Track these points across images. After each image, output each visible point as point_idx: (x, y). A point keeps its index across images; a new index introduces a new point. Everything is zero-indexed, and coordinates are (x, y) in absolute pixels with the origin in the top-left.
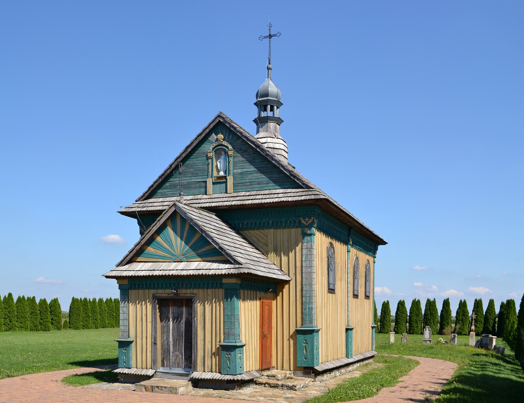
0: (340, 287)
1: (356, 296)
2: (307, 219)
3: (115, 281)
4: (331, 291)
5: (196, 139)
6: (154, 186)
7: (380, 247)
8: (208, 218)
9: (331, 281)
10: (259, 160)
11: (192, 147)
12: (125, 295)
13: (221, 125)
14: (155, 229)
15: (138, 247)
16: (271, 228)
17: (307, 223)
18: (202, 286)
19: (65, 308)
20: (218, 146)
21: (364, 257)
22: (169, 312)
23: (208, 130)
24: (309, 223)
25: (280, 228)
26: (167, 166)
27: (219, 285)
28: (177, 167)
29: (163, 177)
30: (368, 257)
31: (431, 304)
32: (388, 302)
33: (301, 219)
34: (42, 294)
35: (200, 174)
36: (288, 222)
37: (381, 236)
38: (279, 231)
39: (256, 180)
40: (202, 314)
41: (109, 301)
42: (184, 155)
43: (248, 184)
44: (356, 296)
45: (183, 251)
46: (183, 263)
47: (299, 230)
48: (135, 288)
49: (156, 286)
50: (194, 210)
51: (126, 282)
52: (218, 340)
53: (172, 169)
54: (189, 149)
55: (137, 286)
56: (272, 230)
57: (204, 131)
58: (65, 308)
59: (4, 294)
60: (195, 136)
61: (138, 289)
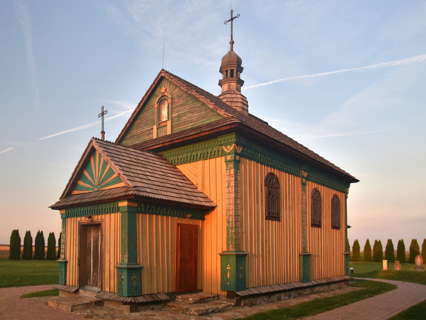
2: (229, 147)
3: (58, 212)
5: (146, 95)
7: (352, 185)
10: (191, 102)
11: (136, 113)
16: (200, 160)
17: (228, 150)
20: (162, 97)
23: (154, 86)
29: (125, 131)
33: (224, 147)
35: (150, 123)
37: (352, 174)
38: (207, 162)
39: (189, 120)
42: (138, 110)
45: (100, 179)
47: (223, 158)
48: (69, 218)
52: (116, 263)
54: (142, 105)
56: (200, 162)
59: (6, 240)
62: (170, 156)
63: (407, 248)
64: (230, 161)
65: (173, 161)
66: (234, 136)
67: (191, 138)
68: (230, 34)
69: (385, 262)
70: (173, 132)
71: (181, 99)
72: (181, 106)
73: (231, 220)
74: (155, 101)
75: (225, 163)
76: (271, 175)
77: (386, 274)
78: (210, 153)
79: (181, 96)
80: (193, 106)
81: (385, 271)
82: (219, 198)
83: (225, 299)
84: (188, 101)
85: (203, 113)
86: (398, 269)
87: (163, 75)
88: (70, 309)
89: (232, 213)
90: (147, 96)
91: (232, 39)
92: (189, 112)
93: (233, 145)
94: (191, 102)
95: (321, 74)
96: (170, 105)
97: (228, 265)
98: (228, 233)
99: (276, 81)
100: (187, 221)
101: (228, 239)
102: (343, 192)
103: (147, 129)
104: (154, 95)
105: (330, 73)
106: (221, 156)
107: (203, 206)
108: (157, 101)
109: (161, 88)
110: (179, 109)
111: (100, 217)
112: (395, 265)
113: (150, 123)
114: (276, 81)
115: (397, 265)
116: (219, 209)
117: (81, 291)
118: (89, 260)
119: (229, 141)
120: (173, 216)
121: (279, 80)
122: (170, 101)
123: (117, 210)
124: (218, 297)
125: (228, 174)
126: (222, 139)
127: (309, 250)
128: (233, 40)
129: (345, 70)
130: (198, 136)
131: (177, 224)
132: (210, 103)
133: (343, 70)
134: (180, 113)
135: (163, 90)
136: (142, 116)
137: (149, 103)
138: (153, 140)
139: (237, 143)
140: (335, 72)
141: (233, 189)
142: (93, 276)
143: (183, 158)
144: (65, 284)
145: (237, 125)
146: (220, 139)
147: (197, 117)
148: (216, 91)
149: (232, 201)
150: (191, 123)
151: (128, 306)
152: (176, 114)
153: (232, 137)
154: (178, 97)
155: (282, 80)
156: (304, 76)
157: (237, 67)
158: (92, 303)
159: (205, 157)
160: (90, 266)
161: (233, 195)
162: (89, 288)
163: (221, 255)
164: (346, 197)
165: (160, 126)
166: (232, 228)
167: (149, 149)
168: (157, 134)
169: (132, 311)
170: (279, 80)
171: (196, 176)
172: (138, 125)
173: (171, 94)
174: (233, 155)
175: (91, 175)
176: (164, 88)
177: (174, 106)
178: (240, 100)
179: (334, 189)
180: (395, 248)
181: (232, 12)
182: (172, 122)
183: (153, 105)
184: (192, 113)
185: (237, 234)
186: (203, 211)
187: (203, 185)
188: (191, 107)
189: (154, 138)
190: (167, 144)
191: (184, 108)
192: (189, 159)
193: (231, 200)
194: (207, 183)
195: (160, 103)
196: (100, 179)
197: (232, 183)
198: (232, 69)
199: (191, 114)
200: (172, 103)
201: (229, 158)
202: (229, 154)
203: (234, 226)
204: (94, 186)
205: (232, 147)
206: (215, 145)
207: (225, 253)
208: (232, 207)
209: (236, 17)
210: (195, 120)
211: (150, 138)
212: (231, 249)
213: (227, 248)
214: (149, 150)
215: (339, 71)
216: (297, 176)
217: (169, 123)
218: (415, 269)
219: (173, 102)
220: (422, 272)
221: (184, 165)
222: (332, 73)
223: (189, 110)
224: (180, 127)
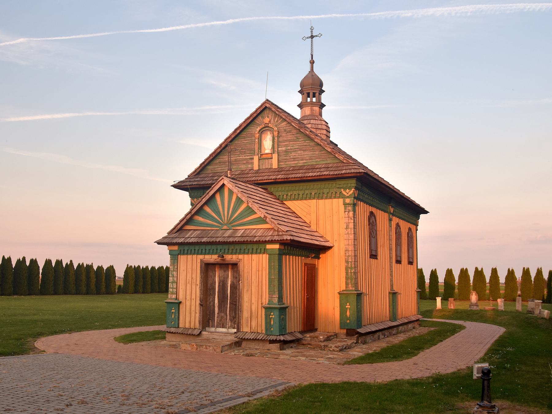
0: (383, 252)
1: (399, 262)
2: (348, 191)
3: (166, 247)
4: (374, 256)
5: (244, 122)
6: (206, 163)
7: (422, 216)
8: (254, 191)
9: (373, 248)
10: (302, 139)
12: (174, 260)
13: (267, 108)
14: (204, 200)
15: (188, 217)
16: (314, 198)
18: (246, 251)
19: (120, 273)
20: (264, 127)
21: (405, 226)
22: (215, 276)
25: (322, 198)
26: (217, 145)
27: (263, 251)
28: (226, 146)
30: (409, 225)
31: (479, 273)
32: (435, 269)
33: (342, 190)
34: (98, 260)
35: (248, 152)
36: (330, 193)
37: (422, 205)
41: (161, 268)
42: (233, 136)
44: (399, 262)
45: (231, 217)
46: (239, 235)
47: (341, 200)
48: (184, 254)
49: (204, 251)
50: (241, 183)
51: (176, 248)
54: (238, 131)
55: (186, 252)
56: (314, 201)
58: (120, 273)
61: (187, 254)
62: (277, 191)
63: (441, 279)
64: (348, 204)
69: (439, 300)
72: (290, 141)
73: (350, 260)
76: (372, 213)
77: (442, 313)
78: (326, 193)
80: (305, 144)
81: (439, 310)
82: (336, 237)
83: (345, 337)
85: (317, 153)
86: (452, 307)
87: (268, 105)
88: (219, 350)
89: (351, 253)
91: (312, 58)
93: (353, 189)
94: (302, 139)
95: (304, 17)
96: (276, 138)
97: (348, 304)
98: (347, 273)
99: (237, 20)
100: (309, 261)
101: (347, 278)
102: (414, 224)
105: (317, 17)
106: (339, 198)
107: (324, 246)
109: (263, 118)
111: (234, 257)
112: (449, 302)
113: (248, 152)
114: (237, 20)
115: (451, 303)
116: (335, 249)
117: (204, 333)
118: (211, 300)
119: (349, 185)
120: (302, 256)
121: (241, 19)
122: (276, 134)
123: (265, 251)
124: (336, 335)
125: (347, 216)
127: (396, 289)
129: (338, 15)
131: (305, 264)
132: (327, 145)
133: (334, 15)
134: (289, 148)
135: (267, 120)
136: (237, 142)
139: (356, 188)
140: (323, 16)
141: (352, 230)
142: (218, 317)
144: (178, 327)
145: (362, 174)
148: (297, 113)
149: (351, 242)
150: (302, 160)
151: (278, 345)
152: (284, 149)
153: (353, 182)
154: (285, 131)
155: (247, 19)
156: (279, 17)
158: (232, 343)
159: (320, 197)
160: (214, 306)
161: (352, 237)
162: (213, 329)
163: (339, 293)
164: (417, 230)
166: (351, 268)
167: (256, 182)
168: (259, 166)
169: (281, 349)
170: (241, 19)
171: (310, 214)
173: (276, 126)
174: (353, 198)
176: (268, 119)
177: (281, 139)
178: (324, 127)
179: (408, 222)
180: (427, 280)
181: (312, 29)
183: (252, 134)
184: (304, 151)
185: (353, 275)
186: (319, 250)
187: (317, 224)
188: (302, 144)
192: (301, 196)
193: (350, 241)
194: (321, 222)
196: (231, 217)
197: (351, 226)
198: (312, 88)
199: (302, 152)
201: (348, 201)
202: (348, 197)
203: (353, 266)
204: (221, 224)
205: (352, 192)
207: (345, 292)
208: (351, 248)
210: (307, 158)
212: (351, 288)
213: (346, 287)
215: (329, 16)
216: (385, 211)
217: (275, 156)
218: (470, 307)
220: (477, 310)
221: (294, 202)
222: (320, 17)
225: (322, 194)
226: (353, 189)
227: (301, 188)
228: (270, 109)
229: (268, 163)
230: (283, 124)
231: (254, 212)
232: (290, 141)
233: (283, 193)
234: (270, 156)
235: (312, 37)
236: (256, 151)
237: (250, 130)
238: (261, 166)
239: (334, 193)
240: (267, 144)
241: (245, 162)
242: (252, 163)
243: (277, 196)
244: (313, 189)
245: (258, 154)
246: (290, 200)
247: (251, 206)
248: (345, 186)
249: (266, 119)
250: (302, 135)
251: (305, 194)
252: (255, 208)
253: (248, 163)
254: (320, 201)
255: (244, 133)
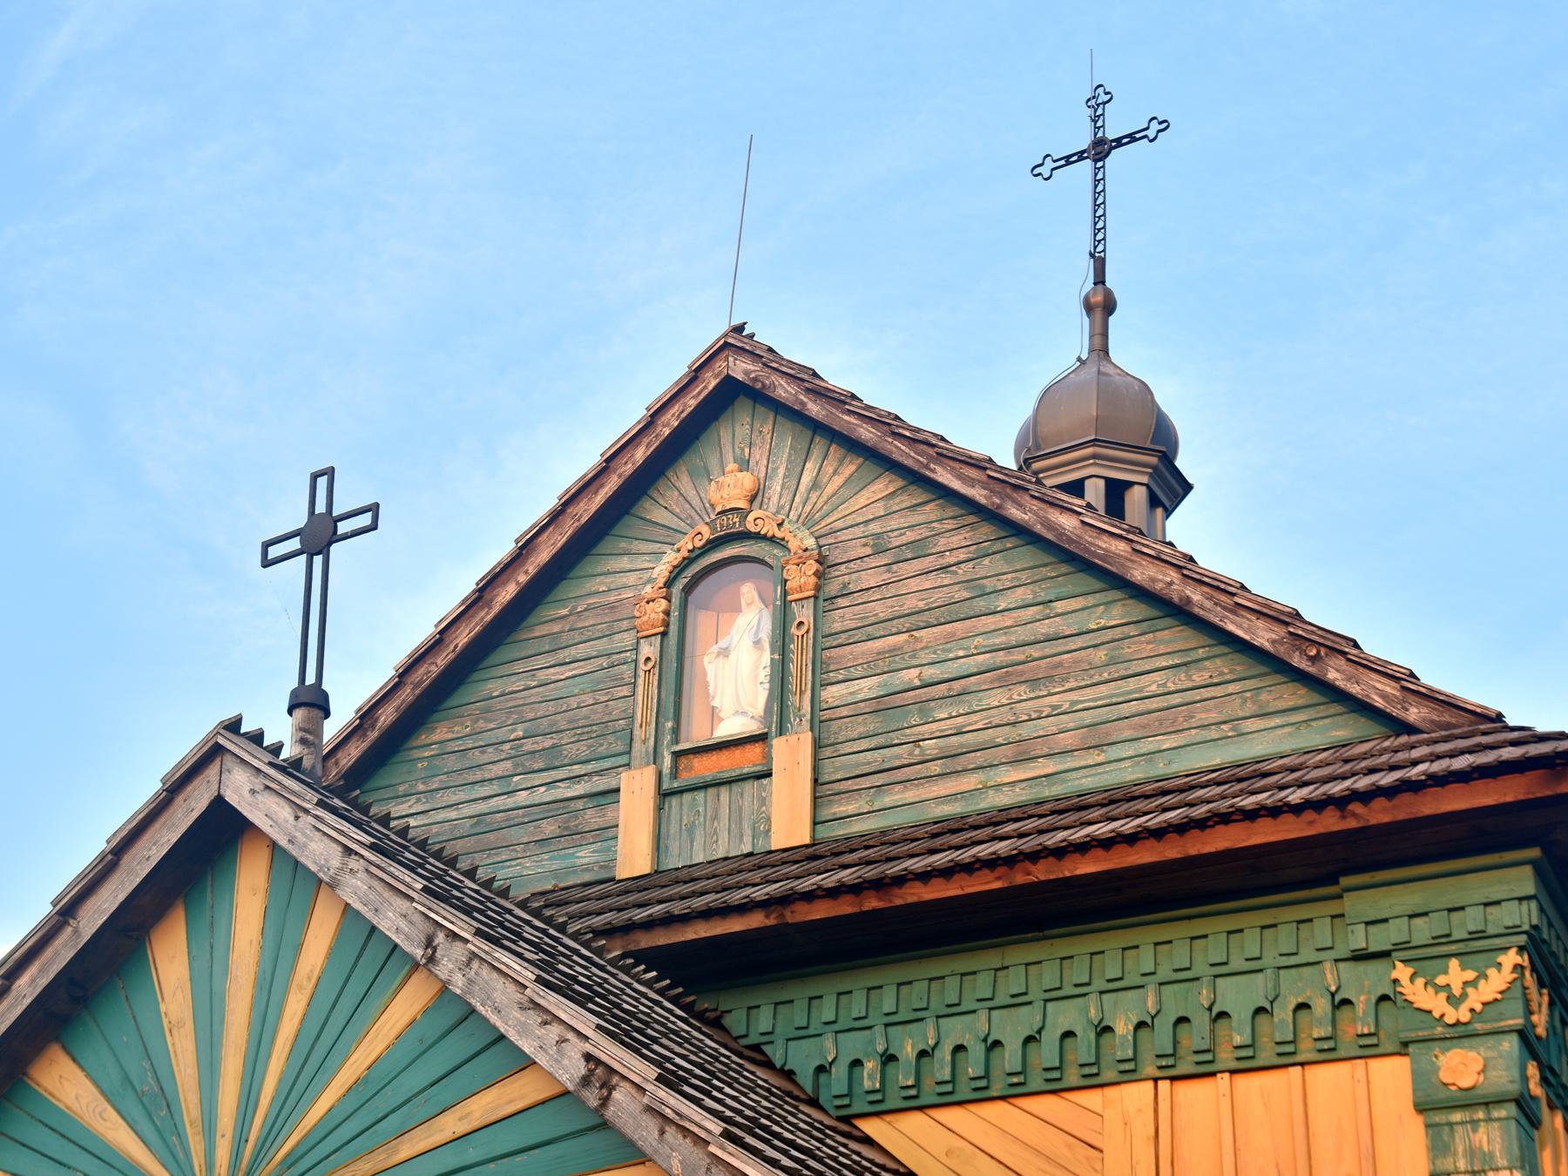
5: (555, 516)
11: (442, 660)
16: (1129, 1073)
17: (1454, 1001)
23: (640, 454)
24: (1475, 1000)
33: (1402, 972)
40: (961, 746)
42: (463, 637)
43: (935, 768)
53: (373, 735)
54: (507, 593)
56: (1137, 1095)
57: (401, 676)
60: (551, 502)
64: (1474, 1101)
65: (840, 1072)
66: (1523, 881)
67: (1086, 866)
68: (1087, 246)
70: (825, 832)
71: (917, 565)
72: (917, 620)
74: (637, 573)
75: (1415, 1126)
79: (918, 549)
80: (1044, 628)
84: (989, 584)
87: (740, 368)
90: (568, 528)
91: (1100, 279)
92: (1004, 675)
93: (1511, 958)
96: (804, 613)
103: (543, 795)
104: (628, 525)
106: (1369, 1049)
108: (662, 570)
110: (894, 651)
113: (582, 750)
122: (802, 577)
126: (1388, 906)
128: (1110, 282)
130: (1171, 850)
135: (730, 487)
136: (495, 687)
137: (566, 590)
138: (607, 887)
143: (945, 1053)
146: (1360, 904)
147: (1088, 718)
152: (867, 687)
153: (1506, 893)
154: (879, 551)
157: (1156, 473)
165: (686, 778)
172: (452, 762)
173: (808, 522)
175: (152, 1105)
176: (747, 480)
177: (839, 620)
181: (1098, 103)
182: (818, 745)
184: (1033, 682)
189: (623, 872)
190: (820, 911)
191: (951, 639)
192: (1010, 1057)
195: (688, 590)
199: (1021, 692)
200: (822, 599)
201: (1461, 1067)
202: (1461, 1034)
205: (1496, 981)
206: (1307, 955)
209: (1068, 160)
210: (1068, 740)
211: (573, 869)
214: (641, 956)
217: (792, 756)
219: (832, 588)
223: (1001, 658)
224: (910, 795)
225: (1201, 1021)
226: (1511, 958)
227: (1013, 982)
228: (758, 396)
229: (737, 815)
230: (862, 499)
231: (499, 1054)
232: (917, 620)
233: (853, 1045)
234: (747, 759)
235: (1100, 150)
236: (644, 735)
237: (599, 584)
238: (674, 847)
239: (1322, 1006)
240: (734, 679)
241: (549, 828)
242: (608, 832)
243: (806, 1080)
244: (1116, 987)
245: (656, 757)
246: (915, 1104)
247: (458, 984)
248: (1423, 930)
249: (740, 473)
250: (1027, 556)
251: (1050, 1038)
252: (504, 992)
253: (573, 835)
254: (1190, 1092)
255: (551, 619)
